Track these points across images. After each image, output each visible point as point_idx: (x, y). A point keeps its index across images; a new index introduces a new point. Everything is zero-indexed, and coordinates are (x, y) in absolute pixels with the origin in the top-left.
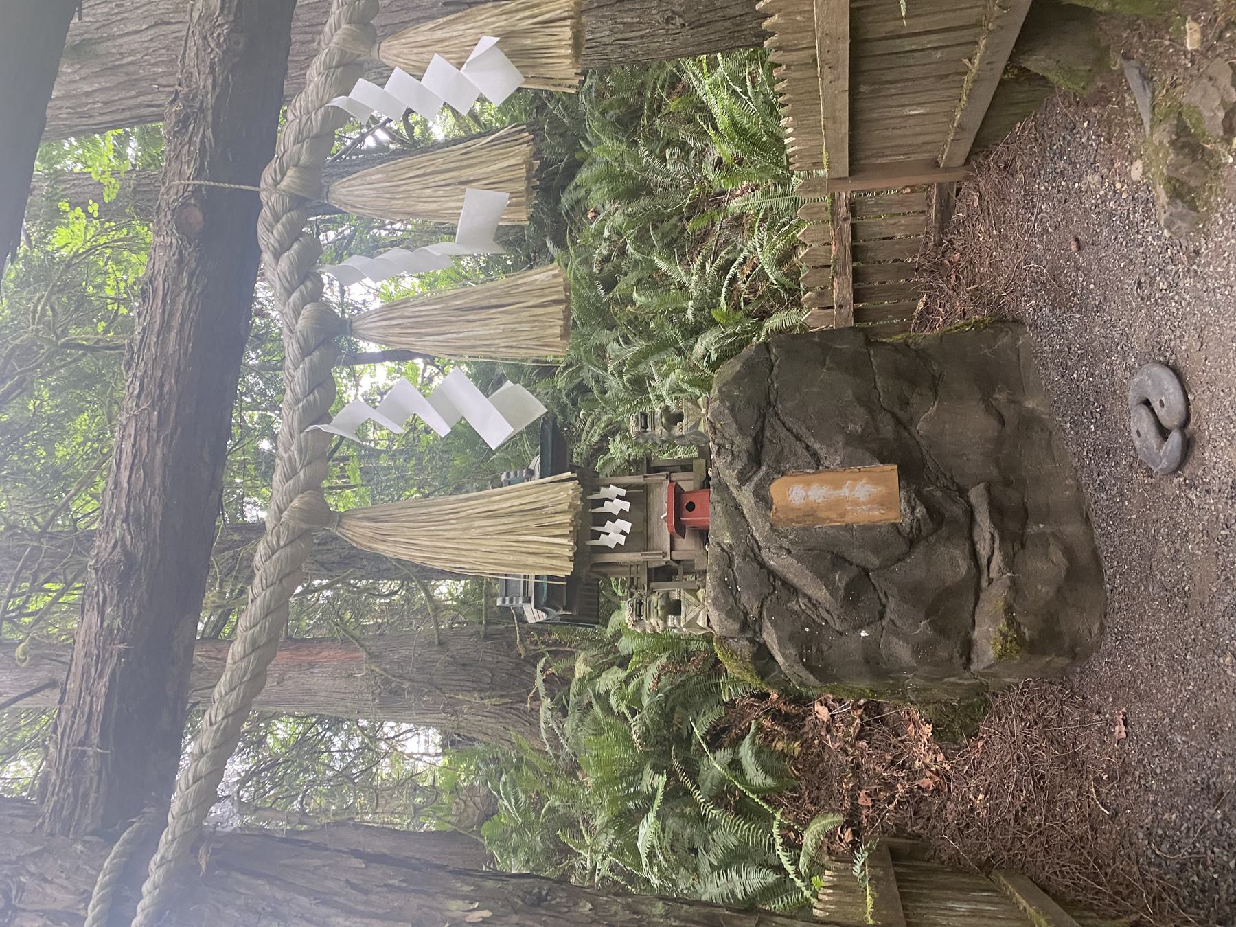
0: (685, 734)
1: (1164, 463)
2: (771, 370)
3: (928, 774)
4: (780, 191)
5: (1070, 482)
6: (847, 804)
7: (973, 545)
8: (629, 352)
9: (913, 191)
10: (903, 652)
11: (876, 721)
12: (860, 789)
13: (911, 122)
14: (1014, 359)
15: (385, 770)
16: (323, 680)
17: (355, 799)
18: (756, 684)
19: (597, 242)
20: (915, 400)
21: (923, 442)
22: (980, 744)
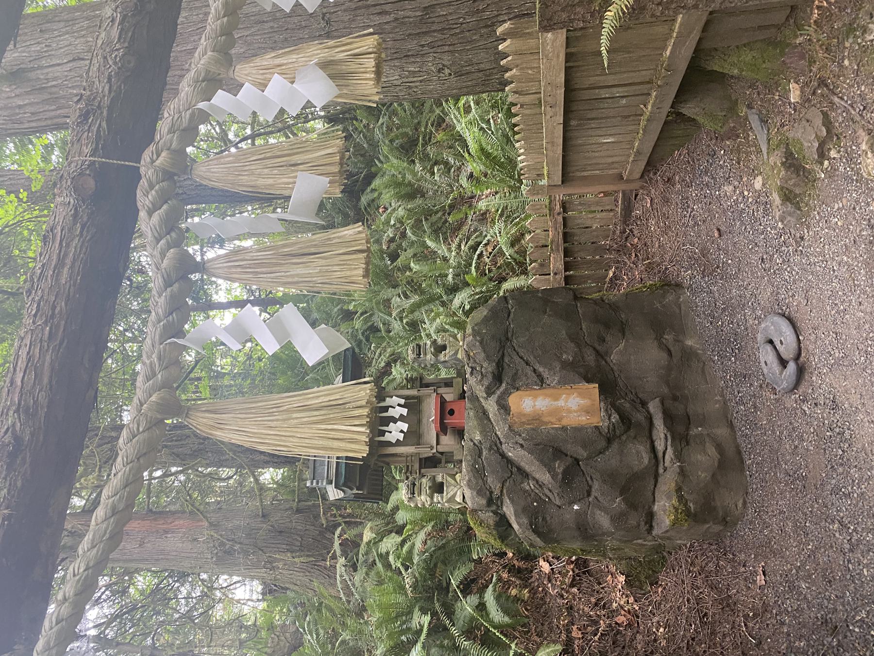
0: (445, 584)
1: (785, 385)
2: (509, 316)
3: (623, 612)
4: (513, 195)
5: (718, 398)
6: (564, 636)
7: (652, 442)
8: (407, 304)
9: (605, 195)
10: (604, 521)
11: (584, 573)
12: (573, 625)
13: (605, 147)
14: (678, 311)
15: (218, 613)
16: (174, 543)
17: (195, 635)
18: (497, 544)
19: (386, 228)
20: (608, 338)
21: (615, 368)
22: (660, 589)
